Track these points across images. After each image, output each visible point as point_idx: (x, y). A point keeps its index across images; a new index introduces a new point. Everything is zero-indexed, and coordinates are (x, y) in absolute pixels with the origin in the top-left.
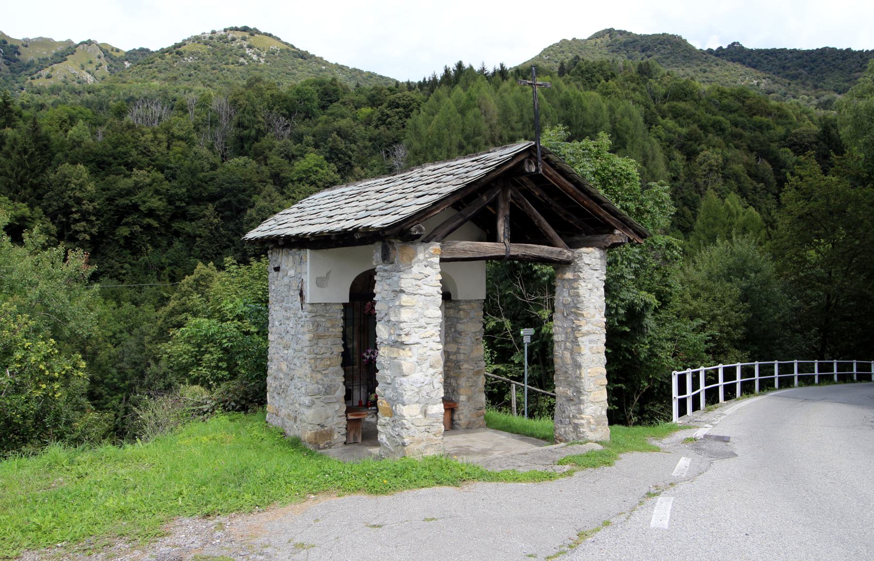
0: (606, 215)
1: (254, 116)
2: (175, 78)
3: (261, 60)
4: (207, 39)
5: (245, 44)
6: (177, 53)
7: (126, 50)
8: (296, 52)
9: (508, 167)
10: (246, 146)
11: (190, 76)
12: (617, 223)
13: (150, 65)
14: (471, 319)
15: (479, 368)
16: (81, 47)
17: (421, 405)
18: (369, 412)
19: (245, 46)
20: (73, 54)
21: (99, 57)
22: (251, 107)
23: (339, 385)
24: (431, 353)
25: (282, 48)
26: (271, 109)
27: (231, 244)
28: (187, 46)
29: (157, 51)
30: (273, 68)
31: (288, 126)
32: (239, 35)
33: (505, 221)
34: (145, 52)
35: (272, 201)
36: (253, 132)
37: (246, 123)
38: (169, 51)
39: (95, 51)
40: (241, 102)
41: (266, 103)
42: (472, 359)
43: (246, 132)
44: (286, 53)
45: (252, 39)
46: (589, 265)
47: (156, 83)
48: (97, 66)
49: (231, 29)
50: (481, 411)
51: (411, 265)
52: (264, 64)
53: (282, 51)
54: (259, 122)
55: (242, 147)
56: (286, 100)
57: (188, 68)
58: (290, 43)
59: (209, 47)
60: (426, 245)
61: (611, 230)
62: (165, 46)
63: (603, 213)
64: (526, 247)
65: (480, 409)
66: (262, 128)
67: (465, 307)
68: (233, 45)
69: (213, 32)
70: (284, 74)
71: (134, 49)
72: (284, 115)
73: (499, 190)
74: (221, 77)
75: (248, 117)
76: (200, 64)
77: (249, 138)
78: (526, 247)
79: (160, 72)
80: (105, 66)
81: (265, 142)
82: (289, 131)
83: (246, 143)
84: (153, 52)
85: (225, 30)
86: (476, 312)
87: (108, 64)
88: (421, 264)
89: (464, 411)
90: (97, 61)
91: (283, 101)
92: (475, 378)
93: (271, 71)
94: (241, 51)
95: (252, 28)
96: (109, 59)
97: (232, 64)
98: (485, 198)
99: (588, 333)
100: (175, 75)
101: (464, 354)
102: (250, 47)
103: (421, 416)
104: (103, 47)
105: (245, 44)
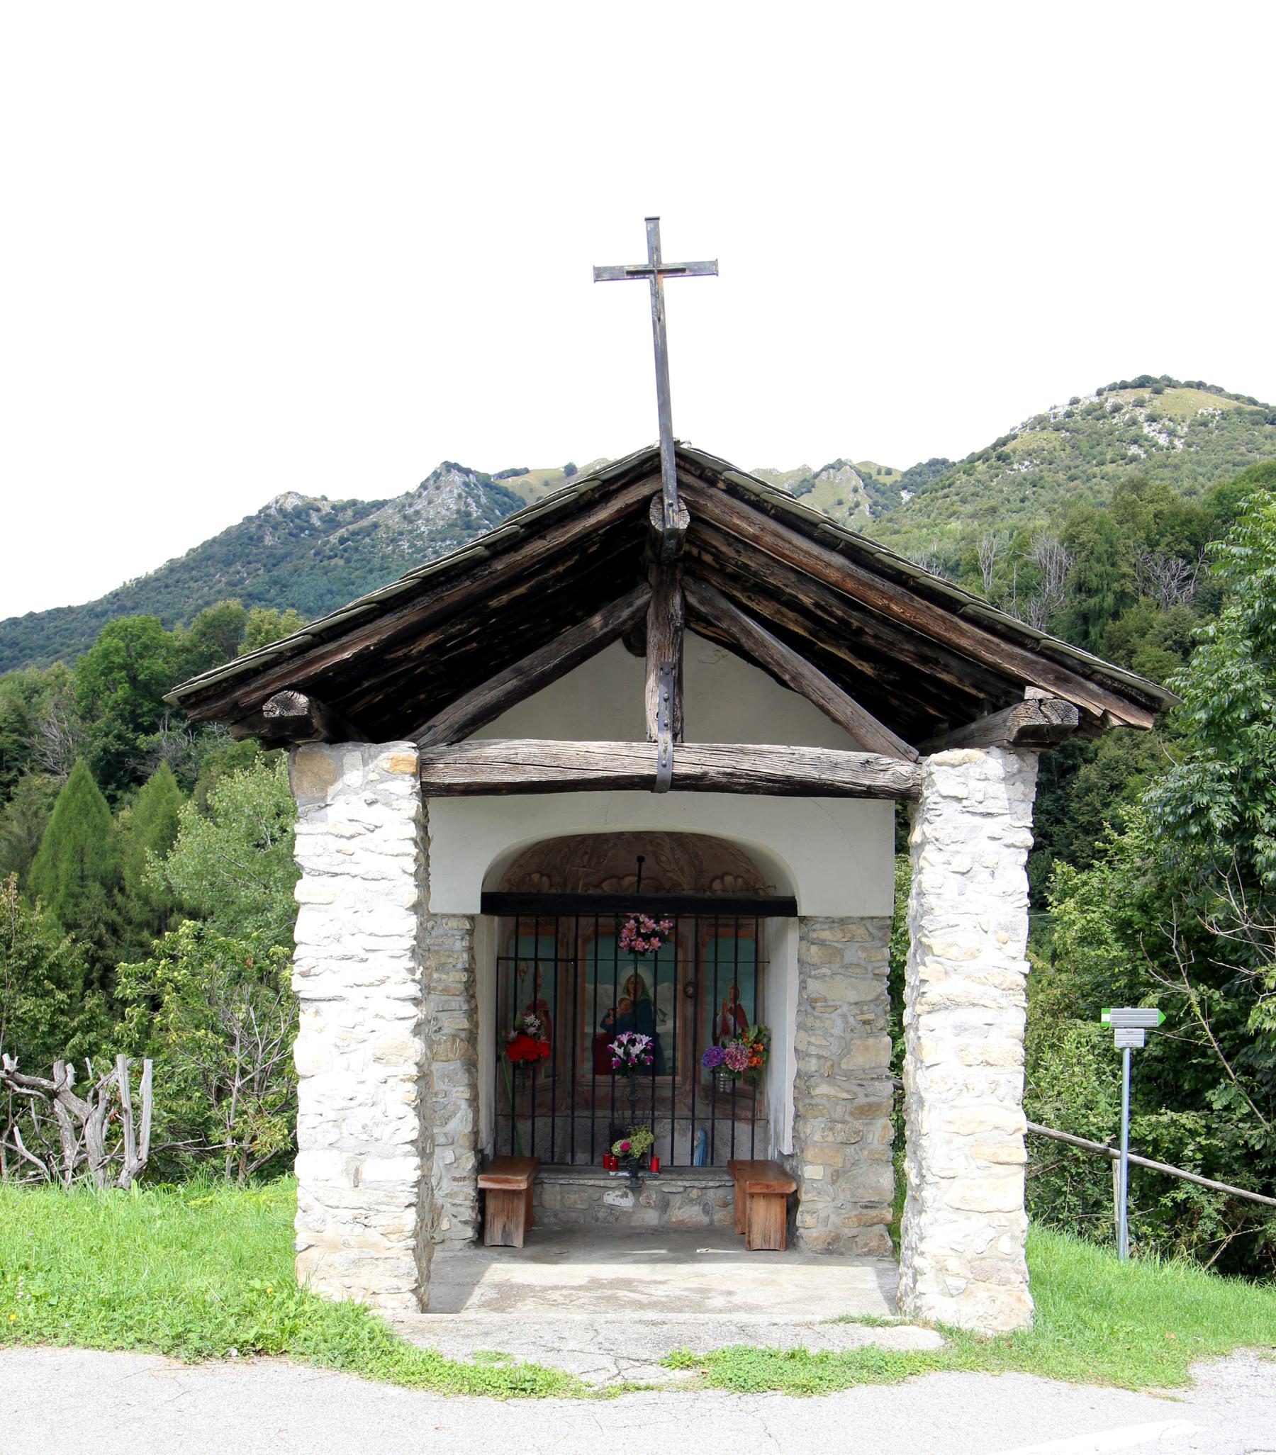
0: (982, 642)
1: (1113, 565)
2: (993, 510)
3: (1177, 442)
4: (1060, 418)
5: (1141, 414)
6: (999, 458)
7: (905, 469)
8: (1257, 413)
9: (578, 528)
10: (1094, 632)
11: (1022, 501)
12: (1027, 664)
13: (946, 491)
14: (847, 966)
15: (871, 1099)
16: (824, 476)
17: (345, 1155)
18: (614, 1184)
19: (1141, 419)
20: (809, 491)
21: (855, 490)
22: (1107, 546)
23: (458, 1107)
24: (377, 1024)
25: (1225, 408)
26: (1153, 544)
27: (1046, 842)
28: (1019, 440)
29: (962, 461)
30: (1204, 458)
31: (1189, 577)
32: (1129, 396)
33: (660, 680)
34: (939, 467)
35: (1137, 746)
36: (1110, 599)
37: (1095, 582)
38: (983, 457)
39: (849, 480)
40: (1083, 538)
41: (1142, 534)
42: (848, 1075)
43: (1093, 601)
44: (1235, 419)
45: (1158, 401)
46: (959, 800)
47: (955, 525)
48: (850, 509)
49: (1113, 388)
50: (873, 1213)
51: (323, 799)
52: (1183, 451)
53: (1224, 416)
54: (1124, 576)
55: (1086, 634)
56: (1190, 521)
57: (1020, 484)
58: (1246, 393)
59: (1064, 434)
60: (373, 748)
61: (1010, 690)
62: (978, 448)
63: (969, 638)
64: (741, 751)
65: (870, 1206)
66: (1130, 588)
67: (826, 935)
68: (1115, 421)
69: (1075, 402)
70: (1229, 466)
71: (920, 465)
72: (1183, 555)
73: (646, 597)
74: (1088, 493)
75: (1098, 568)
76: (1045, 474)
77: (1099, 613)
78: (741, 751)
79: (964, 501)
80: (865, 508)
81: (1132, 617)
82: (1191, 588)
83: (1093, 626)
84: (954, 464)
85: (1099, 393)
86: (864, 949)
87: (870, 501)
88: (353, 798)
89: (820, 1206)
90: (850, 498)
91: (1182, 524)
92: (858, 1124)
93: (1199, 463)
94: (1133, 431)
95: (1158, 377)
96: (872, 492)
97: (1113, 462)
98: (597, 621)
99: (950, 1004)
100: (993, 503)
101: (819, 1057)
102: (1152, 419)
103: (346, 1183)
104: (863, 470)
105: (1141, 414)
